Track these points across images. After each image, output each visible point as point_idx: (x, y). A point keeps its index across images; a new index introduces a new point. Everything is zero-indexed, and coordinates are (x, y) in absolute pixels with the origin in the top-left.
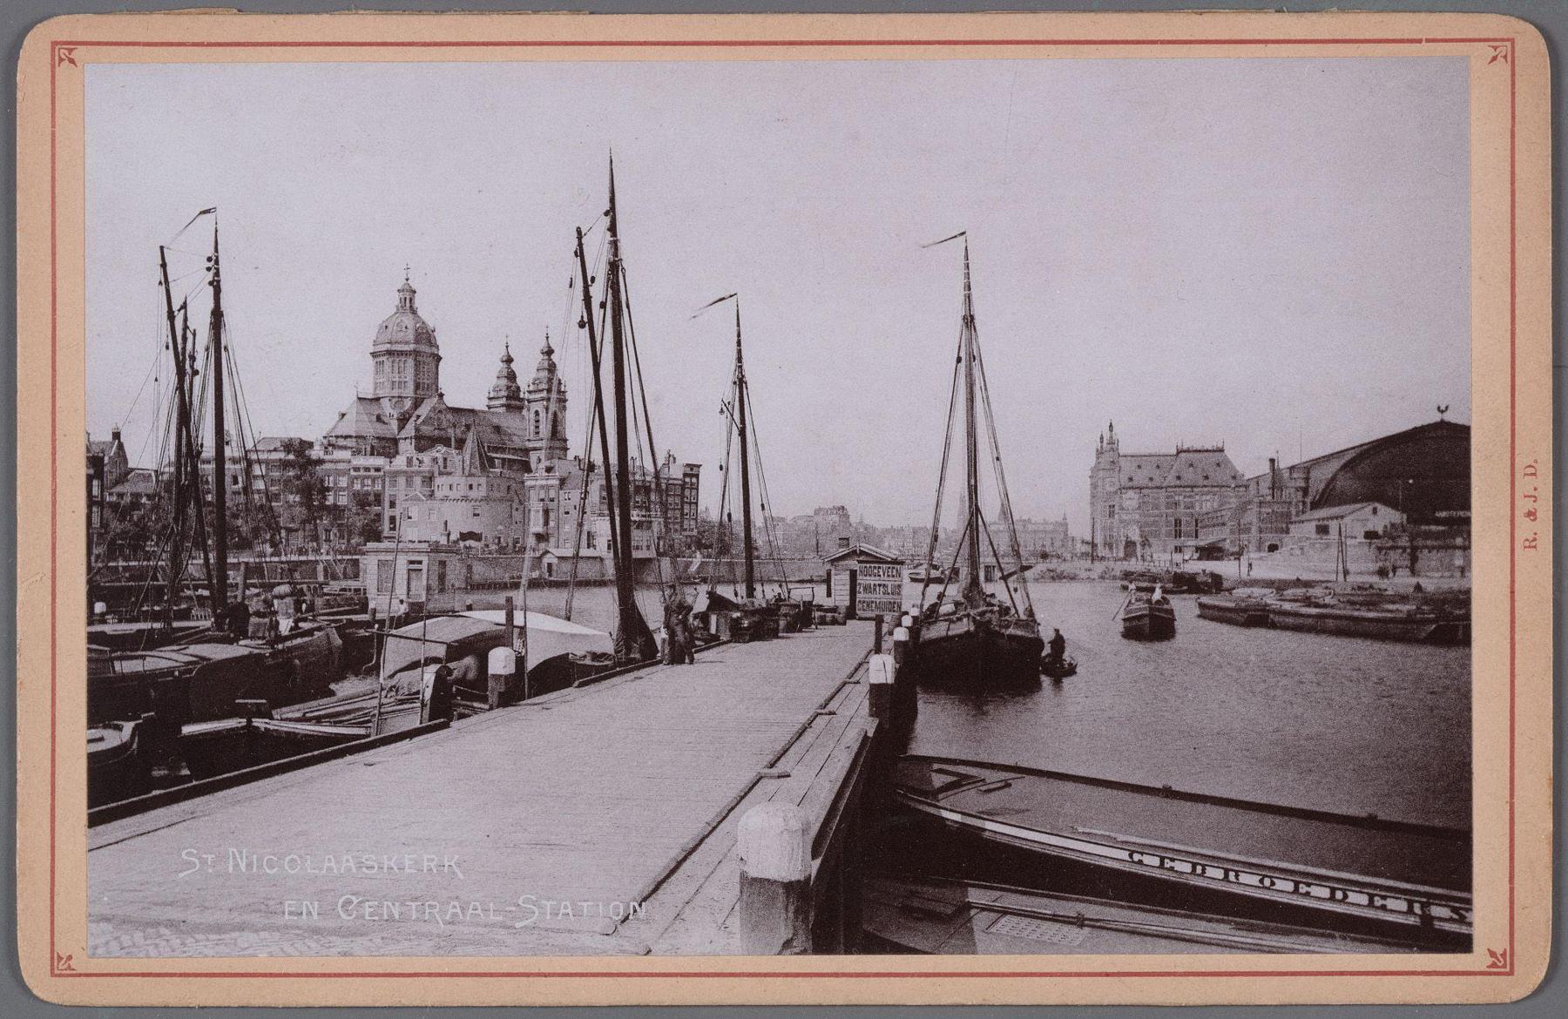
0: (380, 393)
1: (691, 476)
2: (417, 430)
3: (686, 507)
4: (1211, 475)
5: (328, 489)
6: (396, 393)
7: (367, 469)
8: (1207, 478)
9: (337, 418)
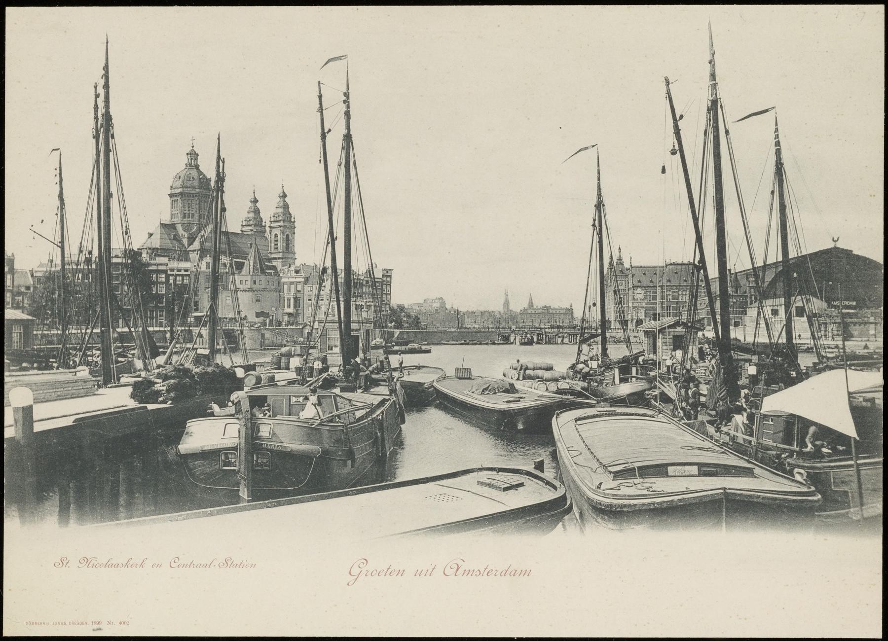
0: (176, 220)
1: (387, 276)
3: (384, 296)
4: (672, 279)
5: (153, 283)
7: (179, 270)
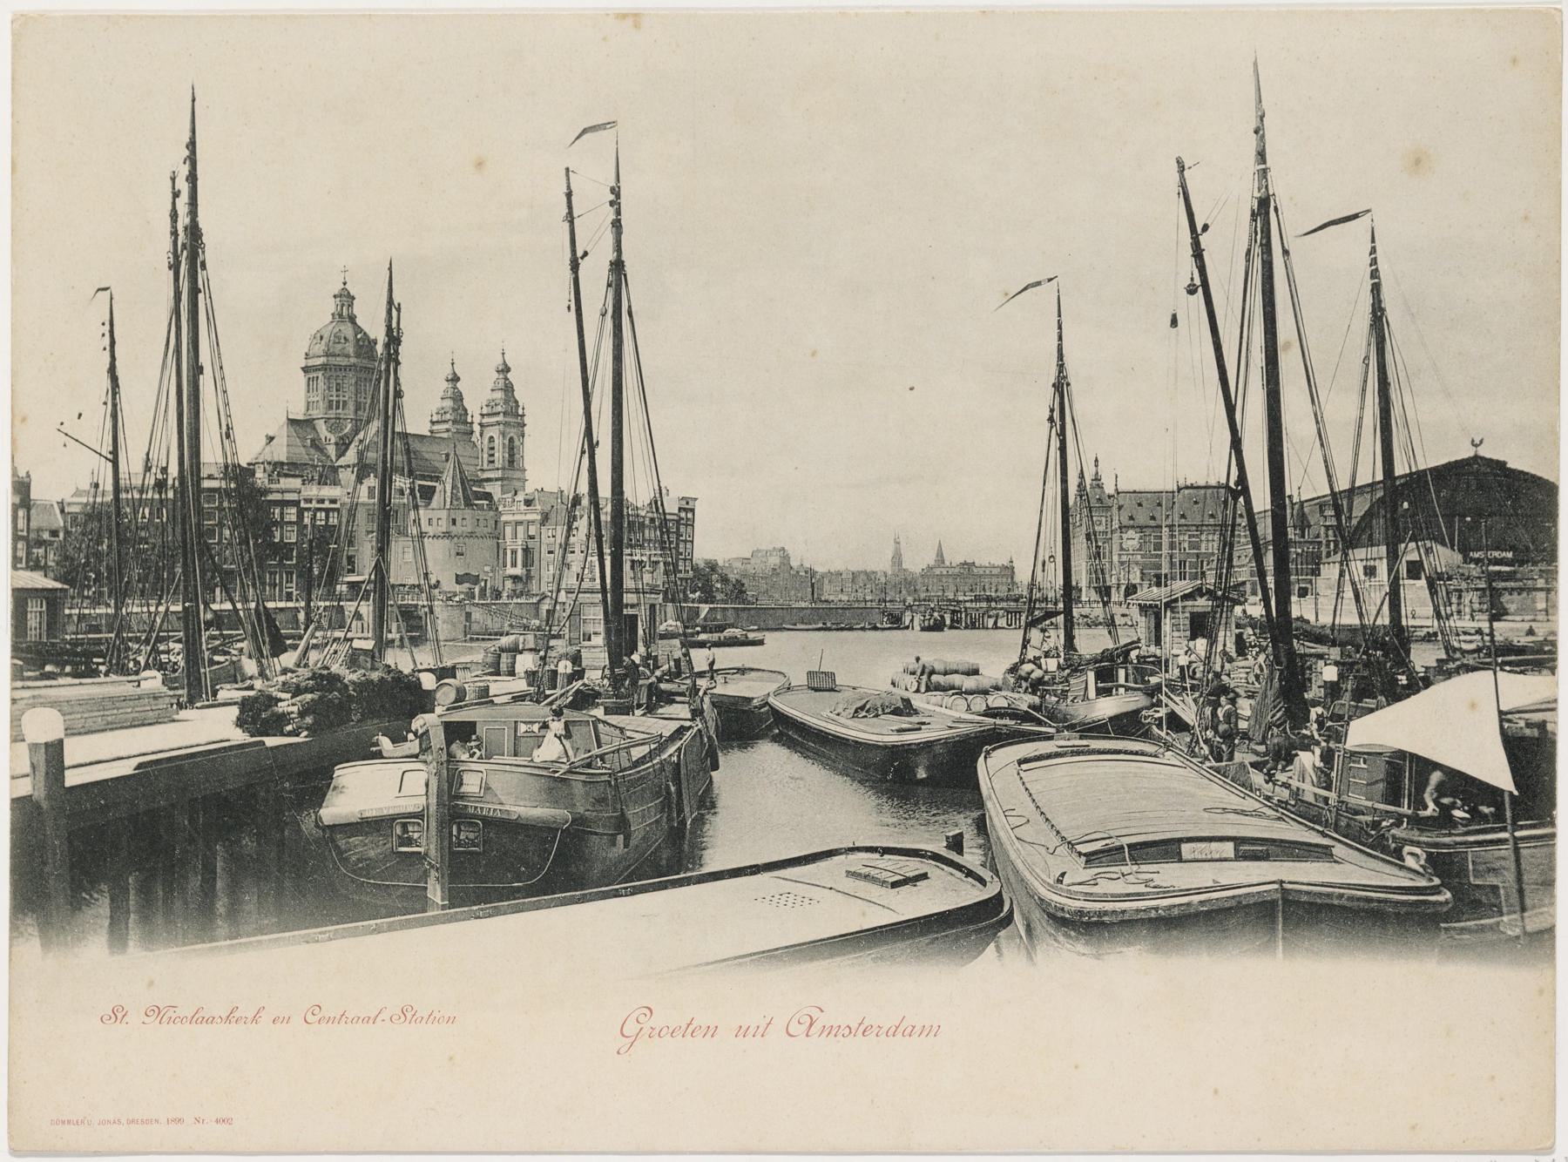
0: (315, 413)
1: (686, 510)
2: (360, 454)
3: (682, 545)
4: (1188, 514)
6: (332, 414)
7: (322, 501)
8: (1131, 518)
9: (264, 441)
